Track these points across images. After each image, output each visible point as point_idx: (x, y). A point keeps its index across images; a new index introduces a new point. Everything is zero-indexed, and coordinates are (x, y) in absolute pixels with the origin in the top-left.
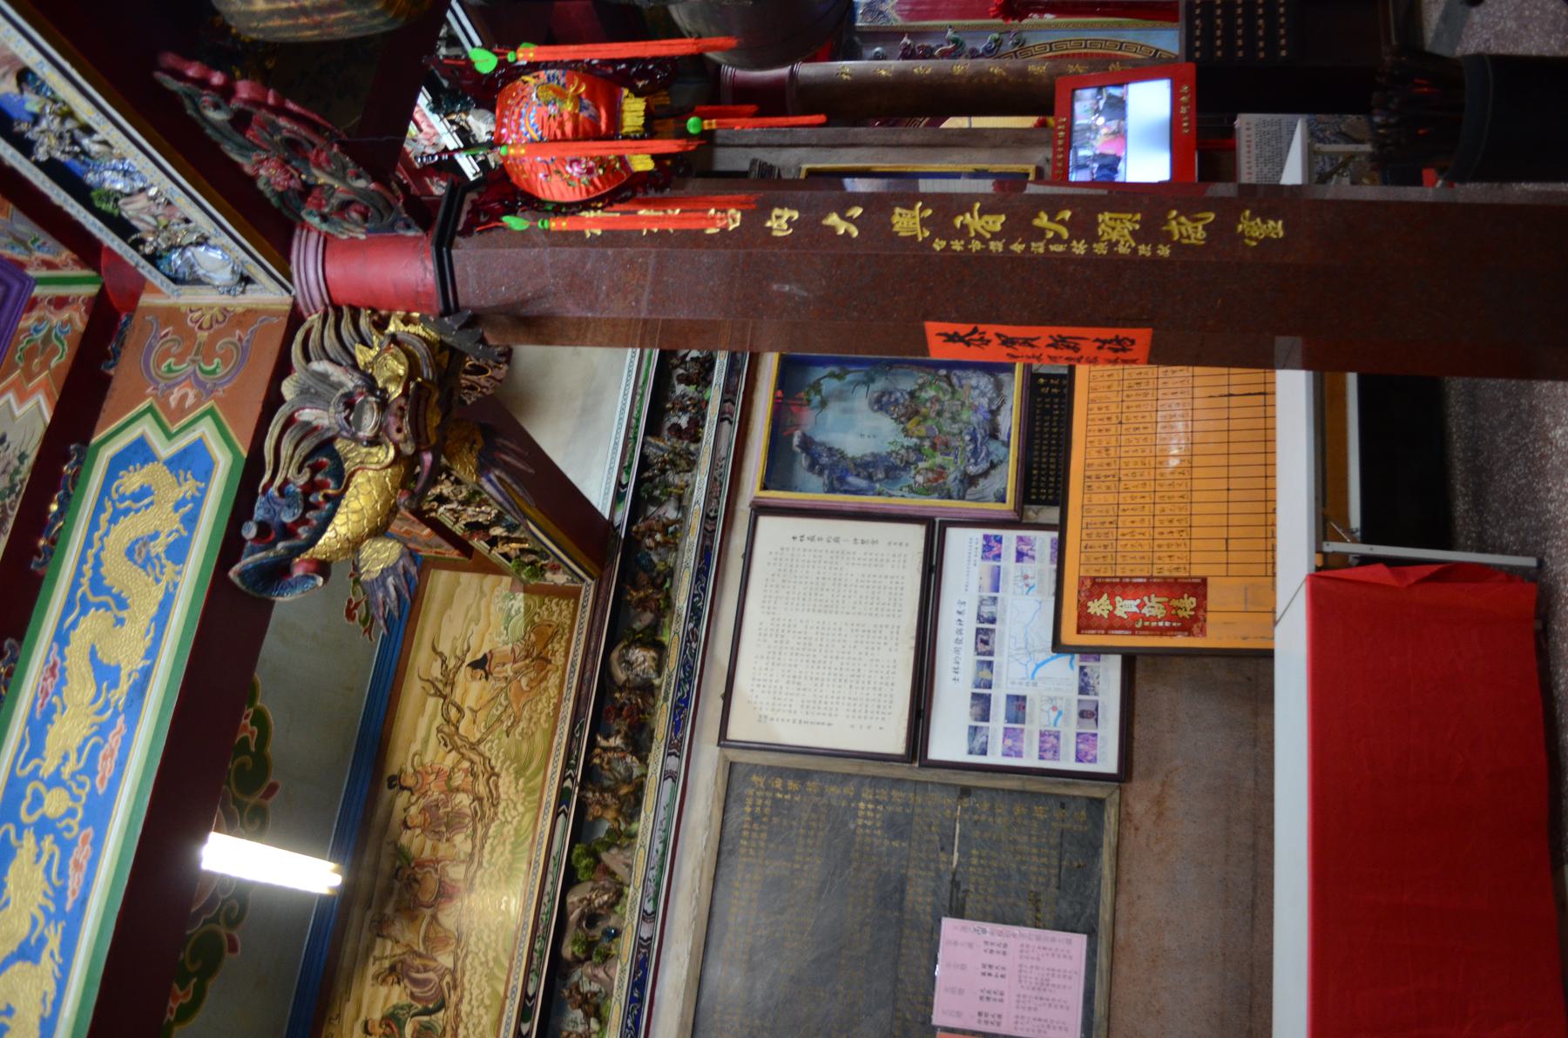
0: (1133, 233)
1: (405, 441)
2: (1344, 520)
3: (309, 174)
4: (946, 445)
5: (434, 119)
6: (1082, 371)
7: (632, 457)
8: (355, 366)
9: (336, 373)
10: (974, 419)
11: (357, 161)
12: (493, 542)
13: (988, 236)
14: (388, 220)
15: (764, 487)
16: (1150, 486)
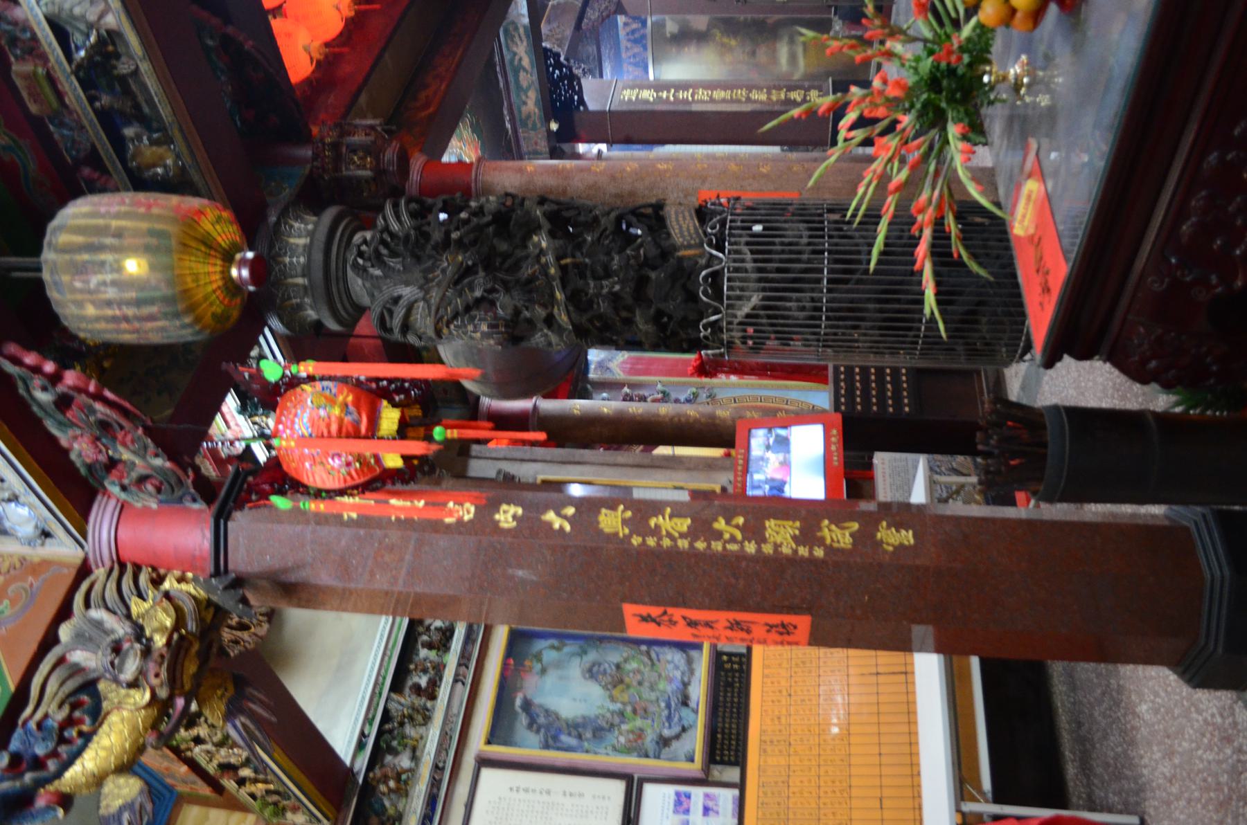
0: (794, 538)
1: (162, 685)
2: (978, 787)
3: (115, 450)
4: (645, 711)
5: (241, 419)
6: (757, 651)
7: (376, 710)
8: (128, 616)
9: (109, 620)
10: (669, 689)
11: (157, 444)
12: (241, 782)
13: (676, 535)
14: (178, 493)
15: (489, 742)
16: (815, 752)
